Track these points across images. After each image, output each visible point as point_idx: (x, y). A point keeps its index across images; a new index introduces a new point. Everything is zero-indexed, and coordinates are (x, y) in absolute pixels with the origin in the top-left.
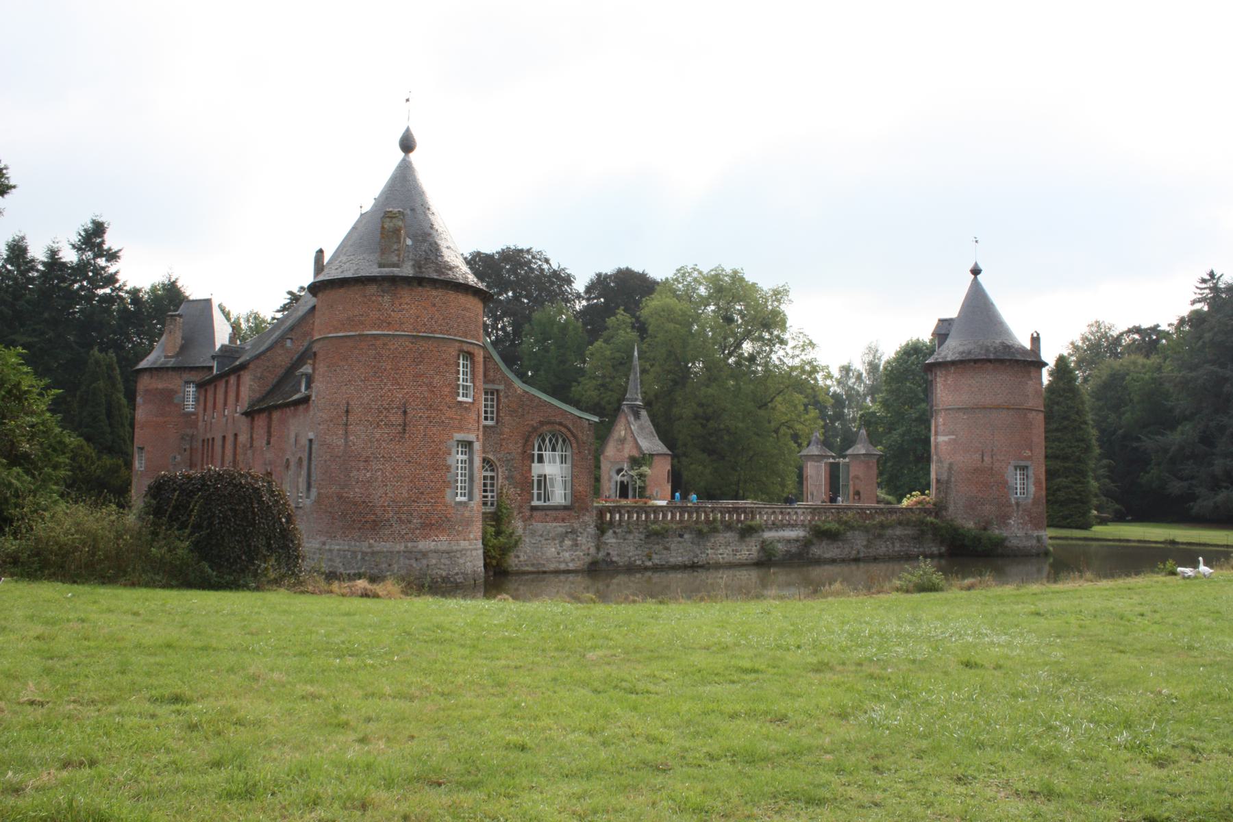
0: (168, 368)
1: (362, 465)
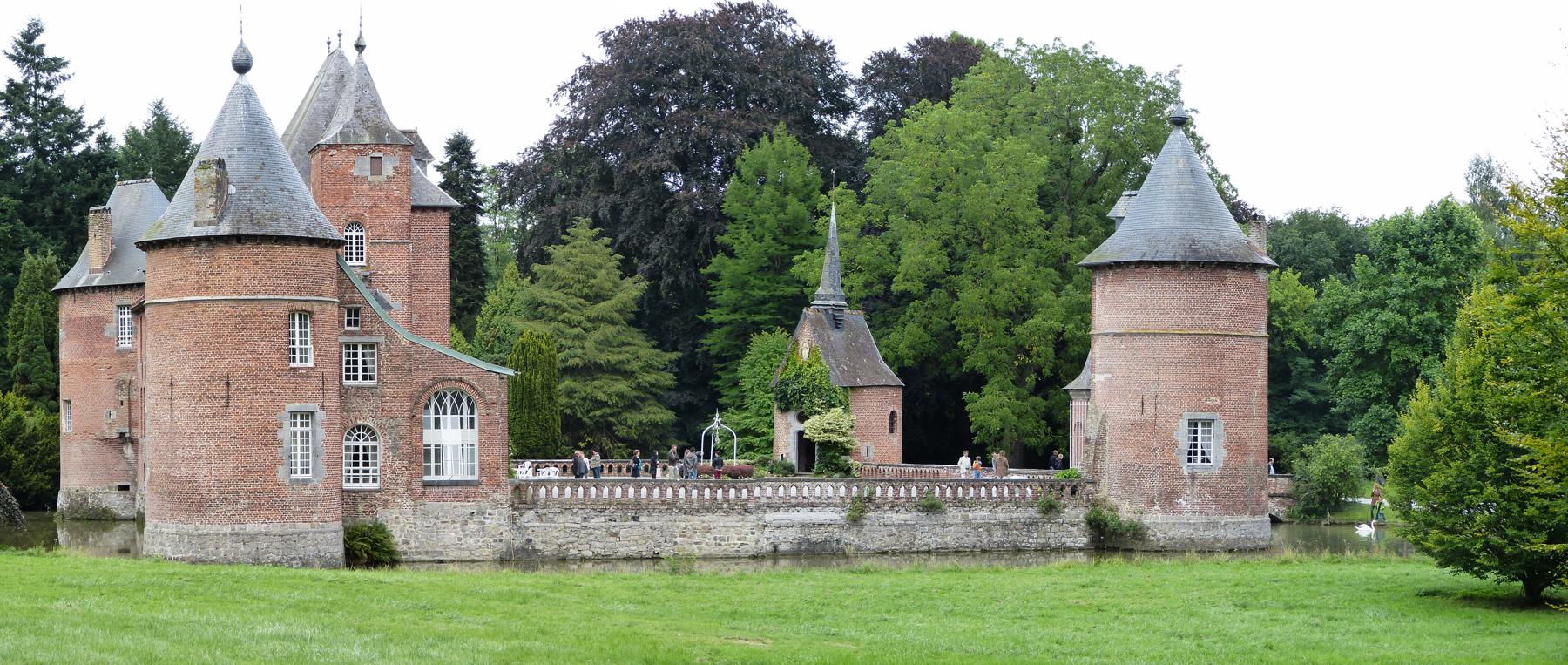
0: (94, 288)
1: (186, 442)
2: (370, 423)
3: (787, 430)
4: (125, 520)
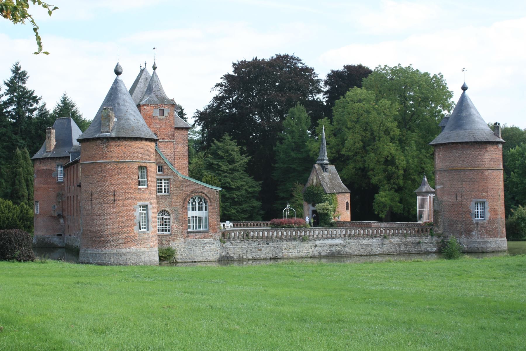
2: (167, 209)
3: (308, 210)
4: (60, 248)
